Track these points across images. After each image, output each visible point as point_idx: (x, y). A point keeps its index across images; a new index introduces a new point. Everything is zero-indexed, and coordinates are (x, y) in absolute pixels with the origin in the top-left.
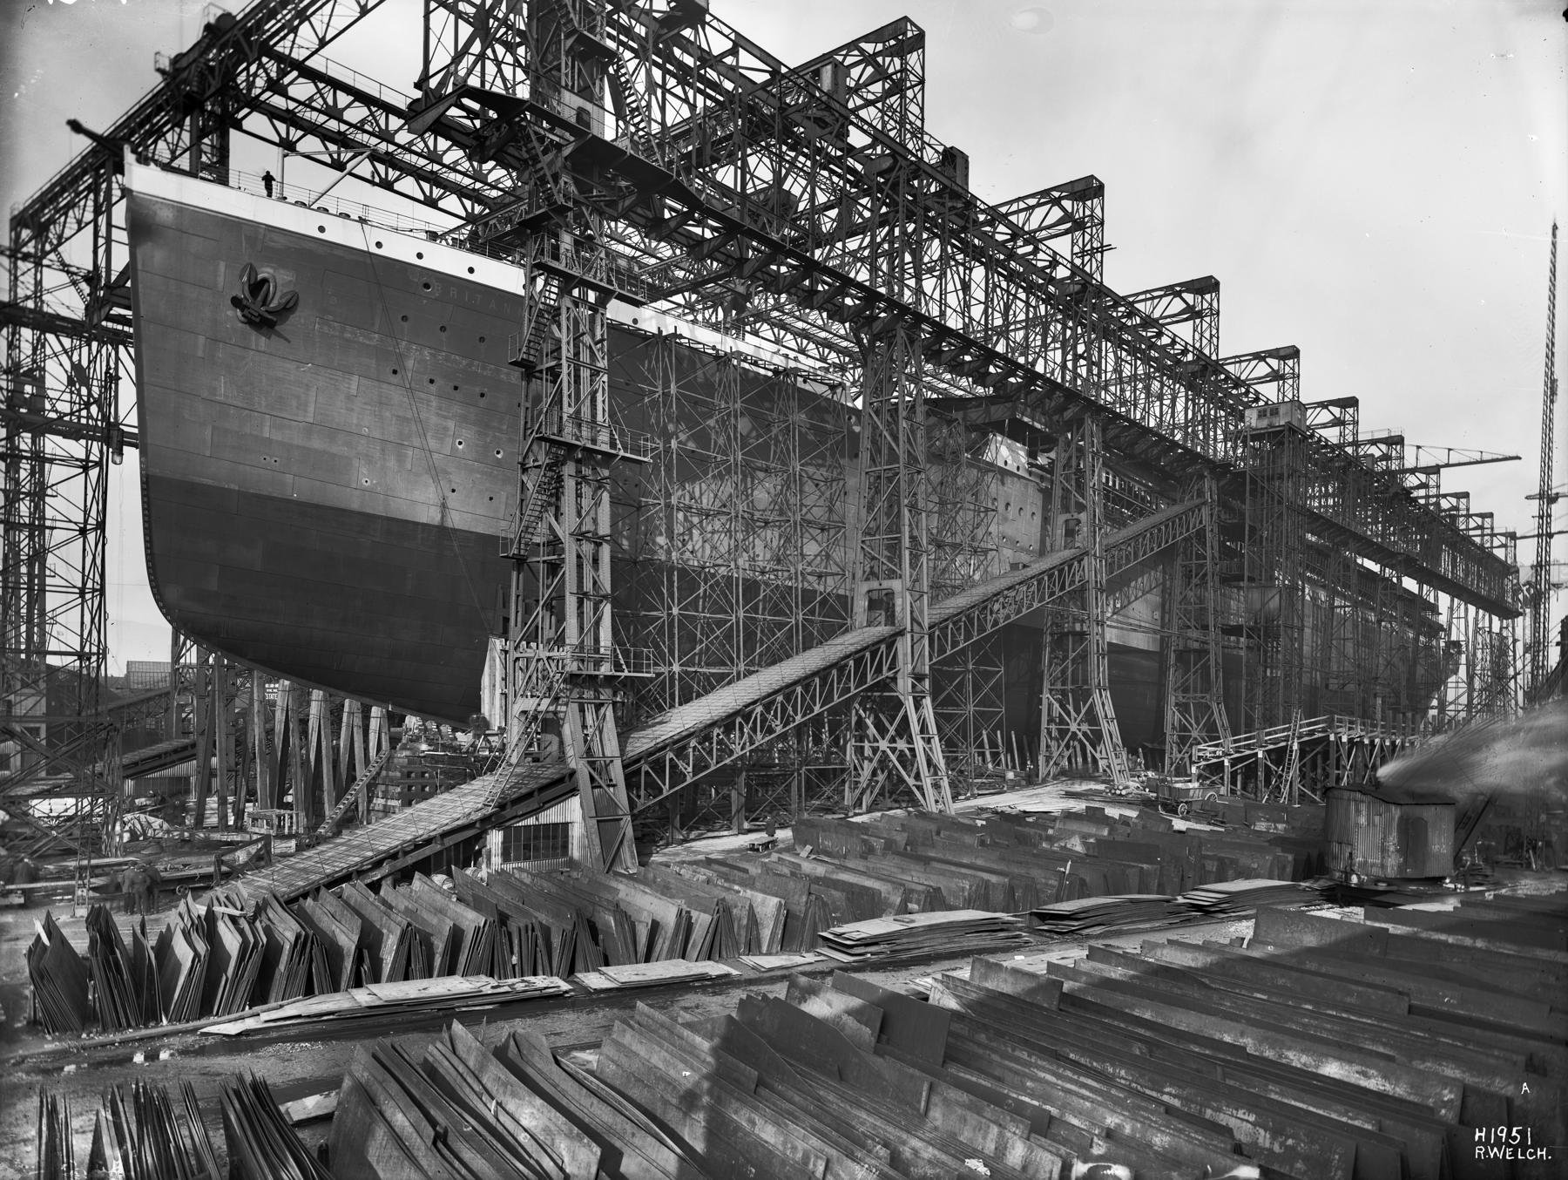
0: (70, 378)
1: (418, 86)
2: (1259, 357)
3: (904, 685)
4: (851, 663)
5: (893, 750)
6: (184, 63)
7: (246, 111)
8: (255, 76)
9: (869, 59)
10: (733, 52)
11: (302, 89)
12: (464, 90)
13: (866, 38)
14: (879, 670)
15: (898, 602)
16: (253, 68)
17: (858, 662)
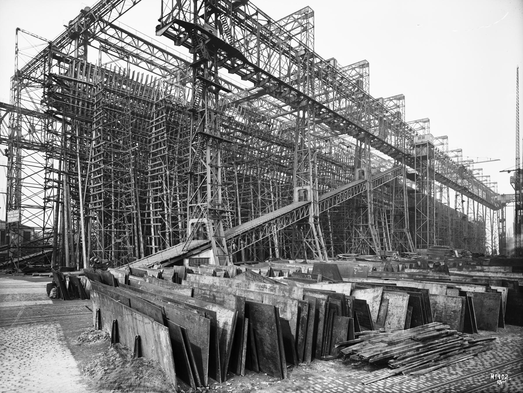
0: (29, 130)
1: (159, 20)
2: (416, 122)
3: (311, 220)
4: (295, 212)
5: (308, 241)
6: (73, 23)
7: (92, 39)
8: (96, 28)
9: (295, 21)
10: (256, 14)
11: (111, 31)
12: (175, 21)
13: (295, 13)
14: (303, 215)
15: (309, 193)
16: (96, 24)
17: (297, 212)
